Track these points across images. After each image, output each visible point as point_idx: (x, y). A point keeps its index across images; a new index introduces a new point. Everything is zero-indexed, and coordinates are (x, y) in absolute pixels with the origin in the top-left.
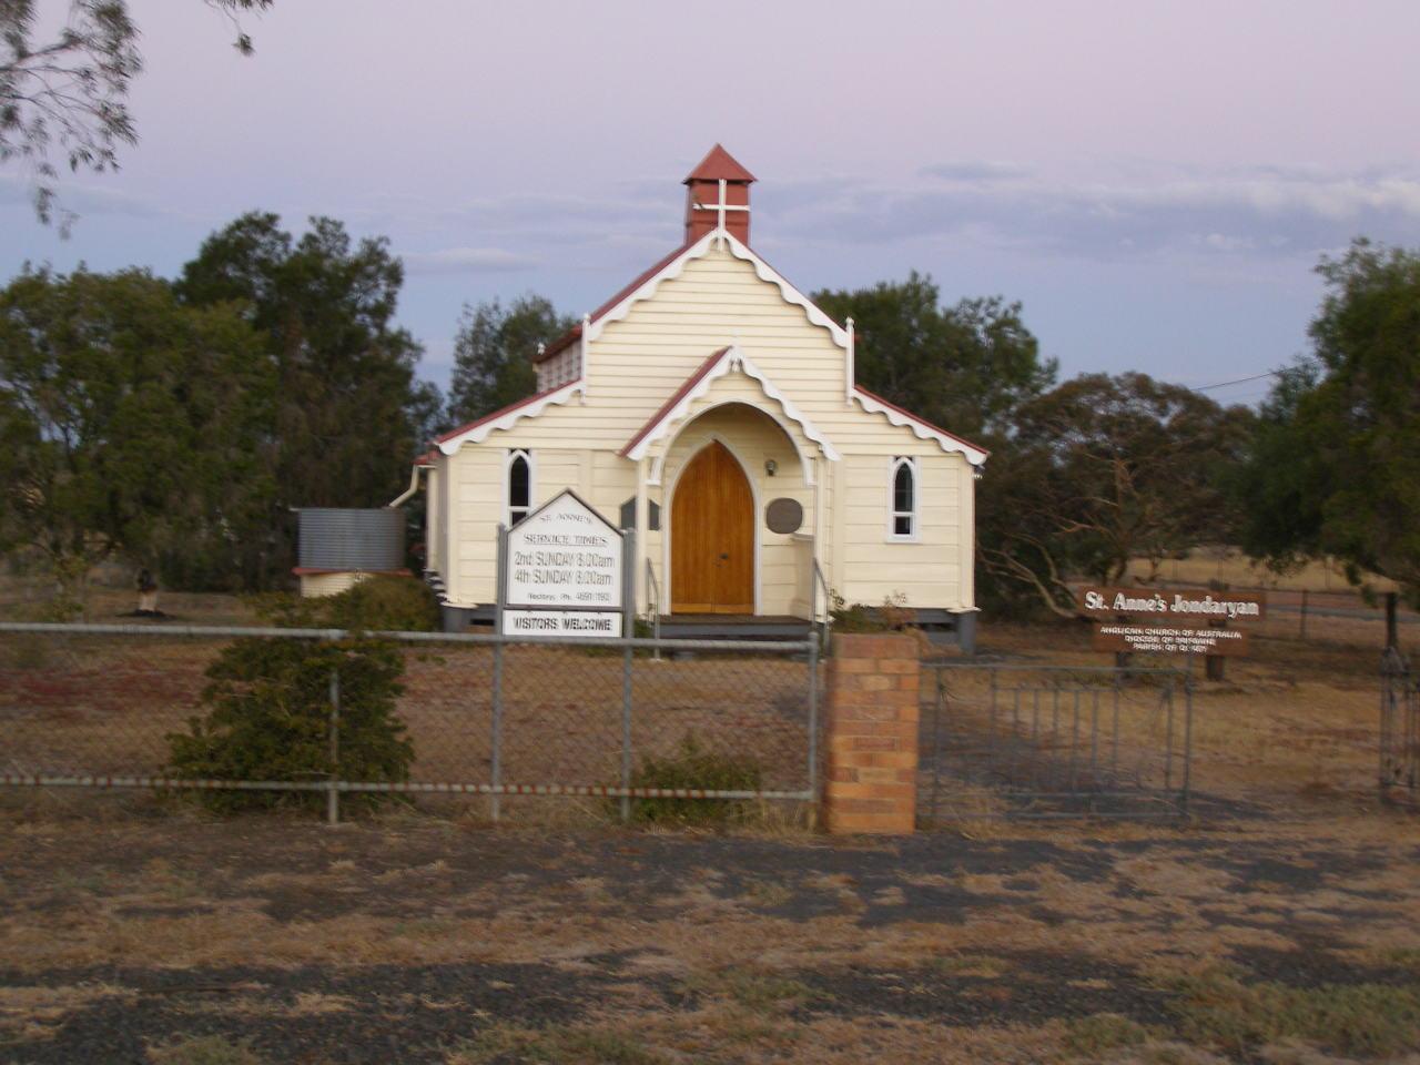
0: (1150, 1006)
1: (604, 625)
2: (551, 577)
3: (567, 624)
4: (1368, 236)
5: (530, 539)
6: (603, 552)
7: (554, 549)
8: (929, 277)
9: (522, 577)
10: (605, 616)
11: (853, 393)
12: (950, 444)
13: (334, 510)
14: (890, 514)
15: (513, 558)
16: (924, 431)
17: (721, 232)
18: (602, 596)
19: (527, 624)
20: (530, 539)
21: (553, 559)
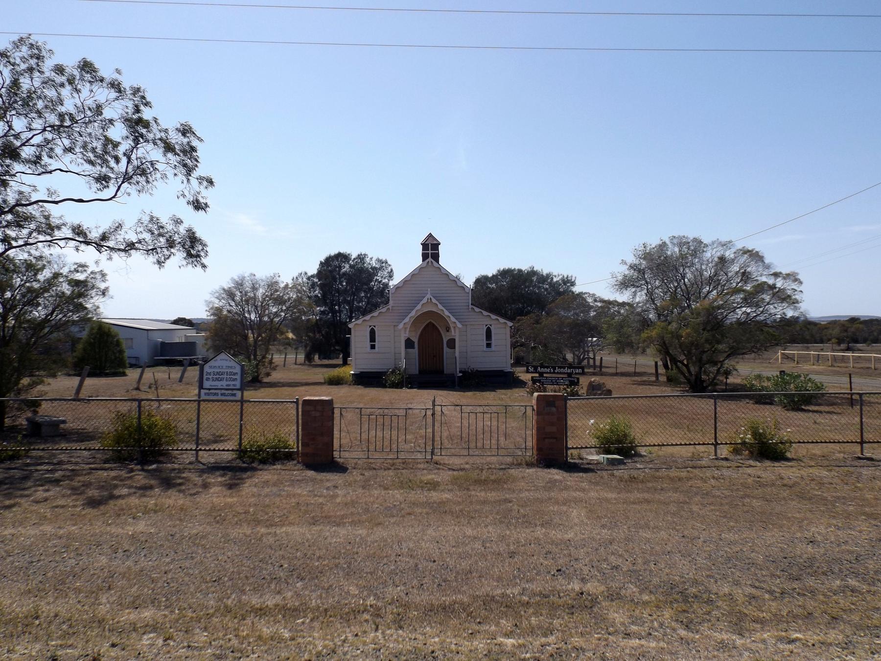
0: (83, 513)
1: (234, 395)
2: (217, 379)
3: (222, 395)
4: (123, 71)
5: (211, 367)
6: (235, 371)
7: (216, 370)
8: (624, 262)
9: (208, 379)
10: (235, 392)
11: (471, 306)
12: (502, 320)
13: (414, 391)
14: (368, 344)
15: (205, 374)
16: (494, 317)
17: (430, 259)
18: (234, 385)
19: (208, 394)
20: (211, 367)
21: (218, 373)
